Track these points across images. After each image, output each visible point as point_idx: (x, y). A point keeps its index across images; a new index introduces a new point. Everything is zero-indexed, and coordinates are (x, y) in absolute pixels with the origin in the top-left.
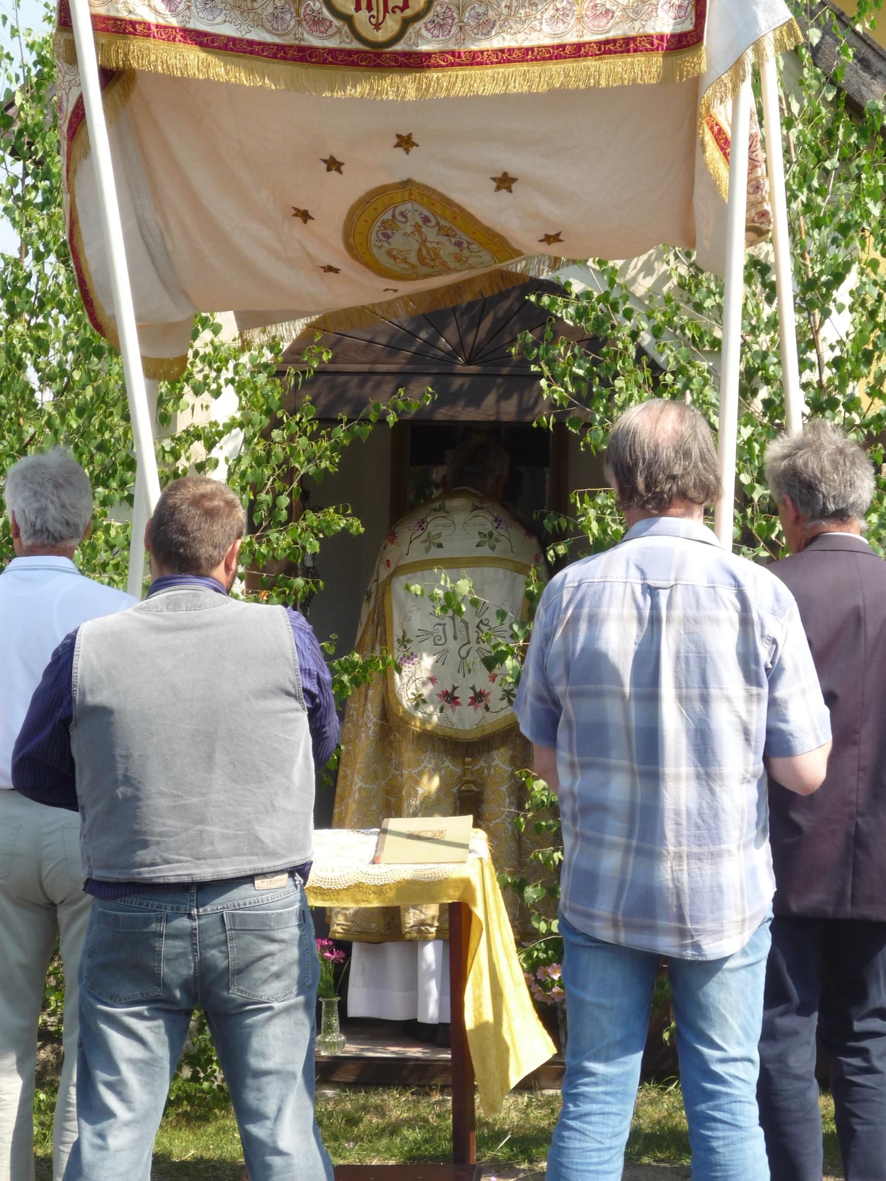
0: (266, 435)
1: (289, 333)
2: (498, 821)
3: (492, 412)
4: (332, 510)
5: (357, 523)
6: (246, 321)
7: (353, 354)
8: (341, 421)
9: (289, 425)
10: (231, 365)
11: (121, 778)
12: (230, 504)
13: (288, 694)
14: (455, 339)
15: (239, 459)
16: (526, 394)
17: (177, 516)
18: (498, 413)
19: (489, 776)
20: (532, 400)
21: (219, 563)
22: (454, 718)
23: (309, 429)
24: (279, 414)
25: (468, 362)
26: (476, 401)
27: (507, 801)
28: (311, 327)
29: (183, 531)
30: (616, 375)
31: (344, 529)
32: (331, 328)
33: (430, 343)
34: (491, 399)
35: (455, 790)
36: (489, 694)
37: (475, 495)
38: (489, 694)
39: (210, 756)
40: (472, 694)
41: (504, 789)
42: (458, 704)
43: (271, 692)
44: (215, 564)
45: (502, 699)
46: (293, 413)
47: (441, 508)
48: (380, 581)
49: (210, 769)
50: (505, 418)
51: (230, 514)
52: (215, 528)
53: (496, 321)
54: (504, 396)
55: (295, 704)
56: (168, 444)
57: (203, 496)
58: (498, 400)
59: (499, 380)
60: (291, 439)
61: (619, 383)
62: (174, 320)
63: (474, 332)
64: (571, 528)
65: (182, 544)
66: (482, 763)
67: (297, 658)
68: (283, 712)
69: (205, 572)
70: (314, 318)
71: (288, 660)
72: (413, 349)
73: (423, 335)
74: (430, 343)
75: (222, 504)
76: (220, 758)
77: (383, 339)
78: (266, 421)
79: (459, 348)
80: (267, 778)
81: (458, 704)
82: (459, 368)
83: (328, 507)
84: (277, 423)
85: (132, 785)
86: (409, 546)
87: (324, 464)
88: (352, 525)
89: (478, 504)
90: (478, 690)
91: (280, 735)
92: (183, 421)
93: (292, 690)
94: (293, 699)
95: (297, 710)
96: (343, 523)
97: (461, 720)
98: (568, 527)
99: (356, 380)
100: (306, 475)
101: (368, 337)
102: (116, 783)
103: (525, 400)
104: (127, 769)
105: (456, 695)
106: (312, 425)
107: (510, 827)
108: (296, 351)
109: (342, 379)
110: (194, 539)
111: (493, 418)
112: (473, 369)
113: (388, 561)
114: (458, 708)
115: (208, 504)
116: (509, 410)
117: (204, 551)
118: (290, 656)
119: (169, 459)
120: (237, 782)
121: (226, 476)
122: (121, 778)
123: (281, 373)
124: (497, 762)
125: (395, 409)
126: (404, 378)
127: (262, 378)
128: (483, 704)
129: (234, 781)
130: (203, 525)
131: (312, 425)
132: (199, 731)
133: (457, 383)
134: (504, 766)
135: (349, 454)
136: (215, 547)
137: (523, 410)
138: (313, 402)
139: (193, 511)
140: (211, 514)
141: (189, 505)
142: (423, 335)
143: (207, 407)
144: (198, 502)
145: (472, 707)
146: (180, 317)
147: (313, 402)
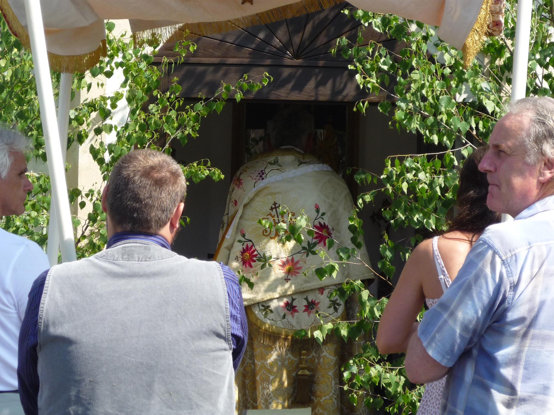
0: (145, 109)
1: (165, 33)
2: (327, 397)
3: (313, 94)
4: (195, 164)
5: (217, 172)
6: (137, 26)
7: (211, 50)
8: (201, 99)
9: (162, 101)
10: (120, 55)
11: (73, 398)
12: (175, 175)
13: (219, 336)
14: (285, 39)
15: (127, 127)
16: (338, 80)
17: (131, 186)
18: (316, 94)
19: (319, 363)
20: (342, 85)
21: (165, 224)
22: (294, 322)
23: (177, 105)
24: (155, 93)
25: (296, 56)
26: (299, 86)
27: (333, 382)
28: (182, 29)
29: (136, 198)
30: (412, 69)
31: (208, 177)
32: (193, 32)
33: (267, 42)
34: (311, 84)
35: (294, 374)
36: (318, 303)
37: (299, 153)
38: (318, 303)
39: (150, 385)
40: (305, 303)
41: (331, 373)
42: (296, 311)
43: (206, 334)
44: (161, 225)
45: (330, 307)
46: (164, 92)
47: (276, 162)
48: (230, 215)
49: (149, 396)
50: (321, 98)
51: (175, 183)
52: (163, 195)
53: (314, 28)
54: (321, 83)
55: (224, 345)
56: (72, 114)
57: (153, 168)
58: (317, 86)
59: (317, 70)
60: (164, 110)
61: (415, 75)
62: (81, 25)
63: (301, 34)
64: (375, 181)
65: (136, 210)
66: (313, 354)
67: (228, 306)
68: (214, 351)
69: (152, 231)
70: (181, 25)
71: (221, 307)
72: (254, 46)
73: (261, 35)
74: (267, 42)
75: (168, 174)
76: (158, 387)
77: (231, 39)
78: (146, 98)
79: (287, 46)
80: (197, 405)
81: (296, 311)
82: (288, 61)
83: (192, 162)
84: (153, 100)
85: (83, 405)
86: (248, 188)
87: (188, 131)
88: (214, 173)
89: (302, 160)
90: (310, 300)
91: (211, 370)
92: (85, 96)
93: (223, 333)
94: (223, 341)
95: (225, 350)
96: (207, 172)
97: (298, 323)
98: (372, 180)
99: (211, 68)
100: (175, 139)
101: (220, 37)
102: (69, 402)
103: (337, 84)
104: (79, 392)
105: (294, 304)
106: (179, 101)
107: (336, 402)
108: (168, 48)
109: (201, 68)
110: (146, 205)
111: (313, 99)
112: (299, 62)
113: (236, 201)
114: (296, 314)
115: (156, 175)
116: (325, 93)
117: (154, 214)
118: (223, 304)
119: (75, 124)
120: (171, 408)
121: (116, 139)
122: (73, 398)
123: (158, 64)
124: (325, 353)
125: (241, 89)
126: (245, 68)
127: (143, 65)
128: (314, 310)
129: (170, 407)
130: (153, 193)
131: (179, 101)
132: (142, 364)
133: (286, 72)
134: (330, 357)
135: (205, 123)
136: (163, 211)
137: (335, 92)
138: (179, 83)
139: (145, 181)
140: (160, 183)
141: (141, 177)
142: (261, 35)
143: (102, 85)
144: (149, 174)
145: (306, 313)
146: (84, 23)
147: (179, 83)
